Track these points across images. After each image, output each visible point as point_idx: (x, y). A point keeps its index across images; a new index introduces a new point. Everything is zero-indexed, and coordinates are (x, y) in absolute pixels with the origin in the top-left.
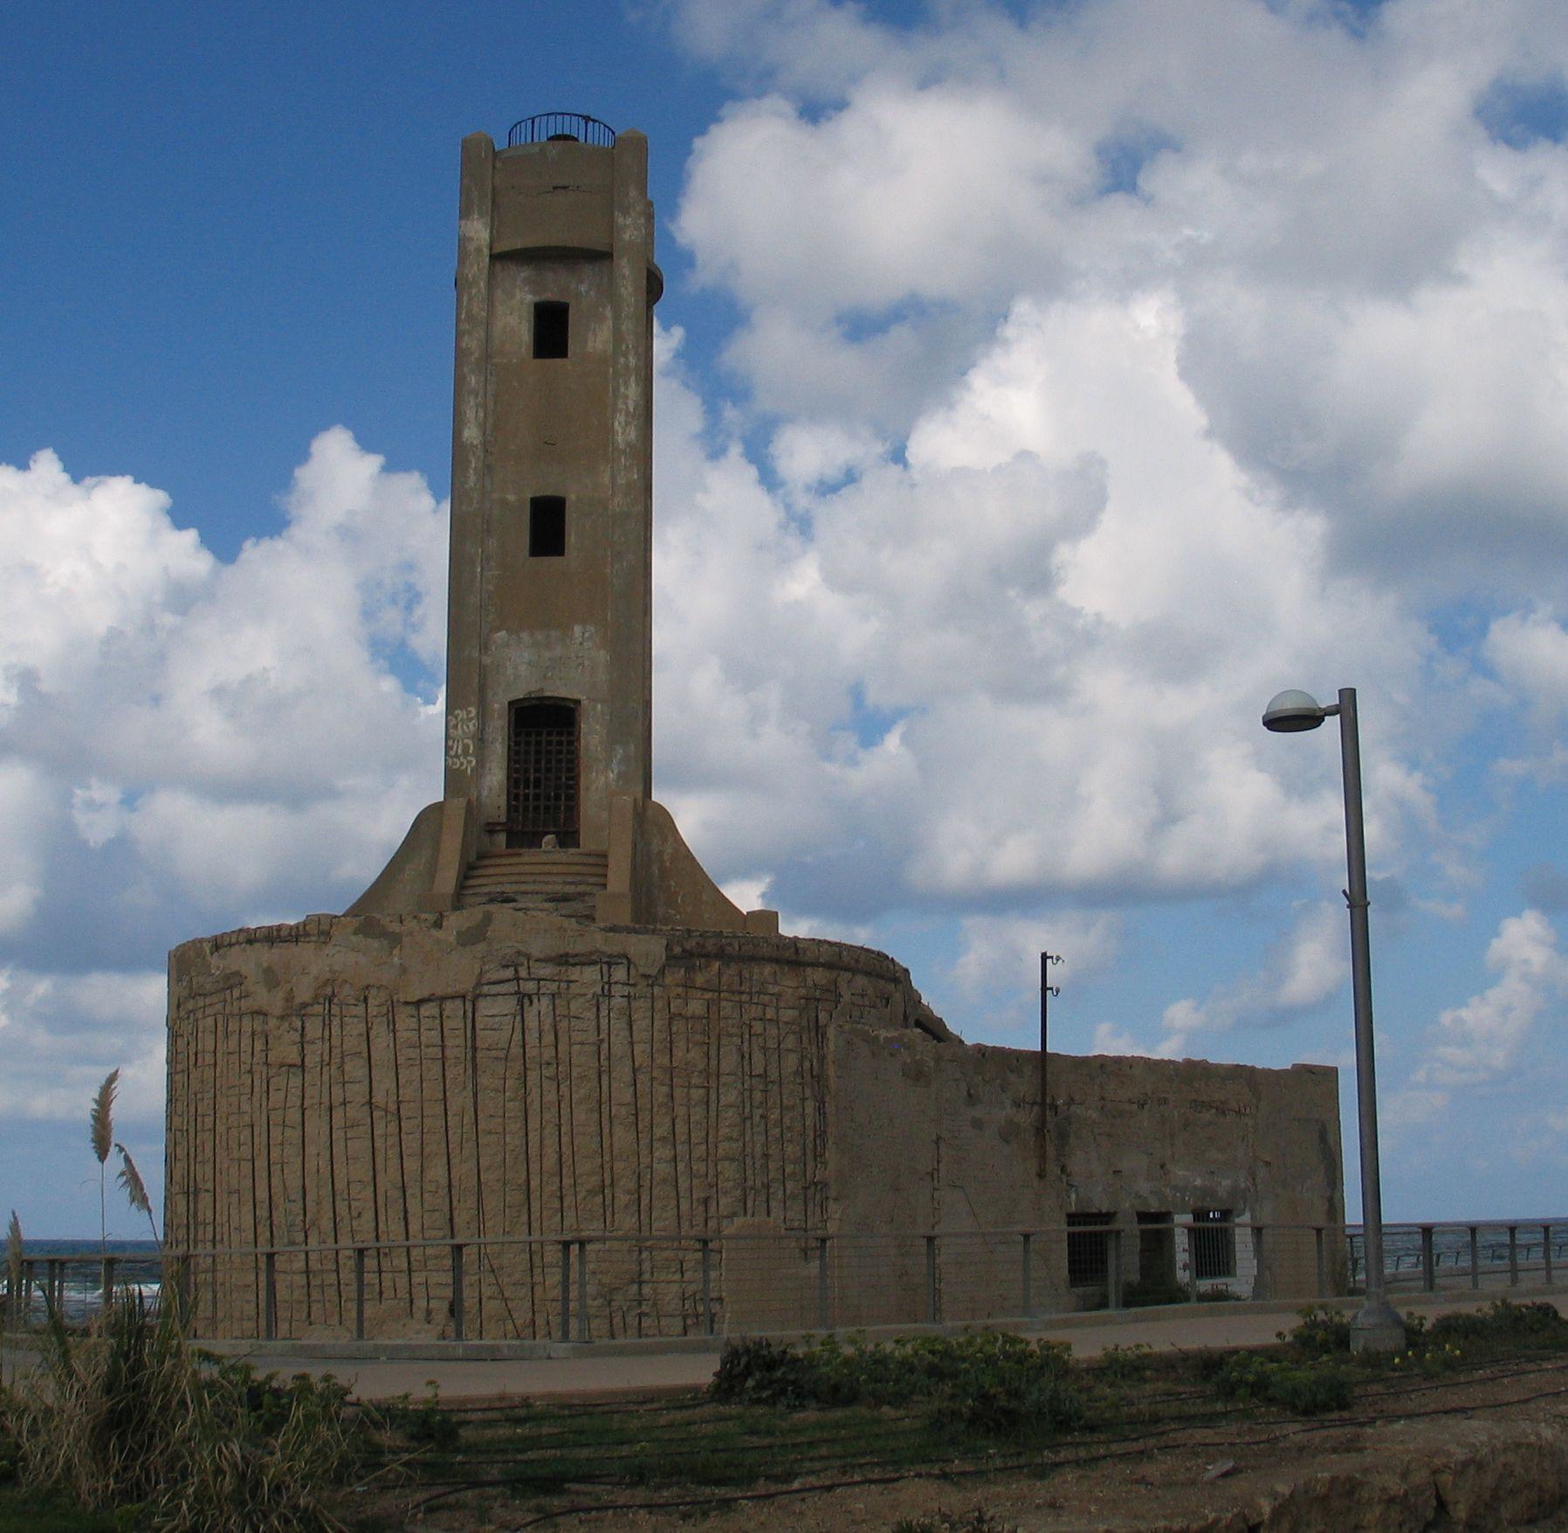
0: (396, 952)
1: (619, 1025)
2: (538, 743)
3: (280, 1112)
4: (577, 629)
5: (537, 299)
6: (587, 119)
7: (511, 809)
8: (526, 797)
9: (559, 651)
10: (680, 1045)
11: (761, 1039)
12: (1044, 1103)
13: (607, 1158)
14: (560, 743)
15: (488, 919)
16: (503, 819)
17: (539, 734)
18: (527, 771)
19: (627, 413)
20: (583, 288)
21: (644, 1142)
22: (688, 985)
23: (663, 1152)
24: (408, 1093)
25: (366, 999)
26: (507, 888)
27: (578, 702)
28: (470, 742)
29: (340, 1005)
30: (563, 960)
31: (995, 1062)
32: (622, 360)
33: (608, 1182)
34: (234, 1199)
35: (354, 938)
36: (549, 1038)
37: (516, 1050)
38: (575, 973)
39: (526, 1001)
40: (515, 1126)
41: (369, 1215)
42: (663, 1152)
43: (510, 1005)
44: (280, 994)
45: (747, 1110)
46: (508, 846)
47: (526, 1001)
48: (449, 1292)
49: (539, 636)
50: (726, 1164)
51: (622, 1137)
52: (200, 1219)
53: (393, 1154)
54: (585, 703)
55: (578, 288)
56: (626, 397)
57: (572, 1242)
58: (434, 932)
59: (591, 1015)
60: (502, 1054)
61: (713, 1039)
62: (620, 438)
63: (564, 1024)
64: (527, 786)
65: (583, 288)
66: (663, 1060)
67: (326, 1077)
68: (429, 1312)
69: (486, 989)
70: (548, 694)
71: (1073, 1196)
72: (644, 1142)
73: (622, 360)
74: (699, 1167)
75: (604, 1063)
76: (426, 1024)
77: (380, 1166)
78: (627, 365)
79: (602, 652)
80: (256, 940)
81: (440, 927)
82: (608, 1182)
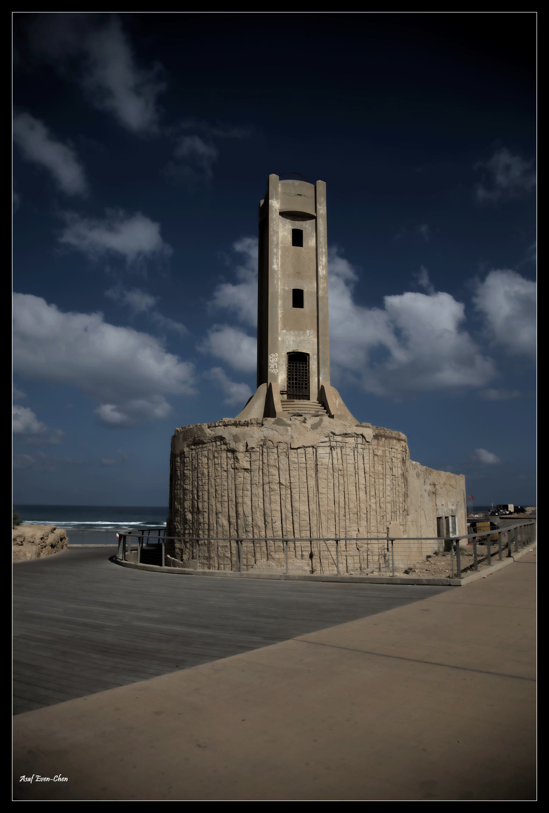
1: (360, 458)
2: (296, 366)
4: (308, 331)
5: (293, 228)
7: (288, 387)
8: (293, 383)
9: (302, 338)
10: (376, 464)
14: (303, 367)
16: (286, 390)
17: (296, 364)
18: (293, 375)
19: (323, 266)
20: (307, 226)
22: (378, 445)
26: (300, 412)
27: (308, 355)
29: (267, 448)
30: (346, 435)
36: (340, 461)
37: (330, 466)
38: (348, 440)
40: (331, 492)
42: (373, 500)
43: (328, 450)
49: (296, 333)
51: (362, 494)
54: (311, 355)
55: (306, 226)
58: (303, 424)
59: (352, 454)
60: (326, 467)
63: (344, 457)
64: (293, 380)
65: (307, 226)
66: (372, 469)
68: (302, 556)
70: (299, 351)
74: (382, 505)
75: (357, 470)
76: (300, 456)
78: (322, 252)
80: (228, 425)
81: (305, 422)
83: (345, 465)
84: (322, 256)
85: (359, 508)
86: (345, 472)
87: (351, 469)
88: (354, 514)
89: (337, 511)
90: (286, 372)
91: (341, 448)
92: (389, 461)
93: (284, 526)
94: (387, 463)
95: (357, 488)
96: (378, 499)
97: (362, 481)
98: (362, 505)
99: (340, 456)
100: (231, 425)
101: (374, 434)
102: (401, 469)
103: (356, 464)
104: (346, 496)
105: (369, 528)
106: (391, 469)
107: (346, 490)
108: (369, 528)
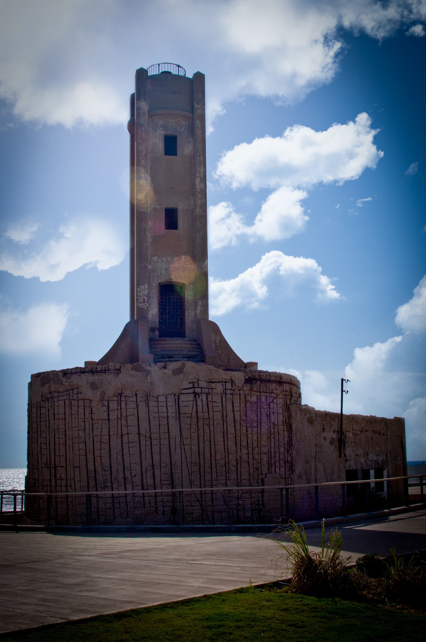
0: (148, 377)
2: (170, 299)
3: (99, 437)
5: (165, 133)
6: (179, 66)
8: (166, 318)
11: (272, 409)
12: (341, 432)
13: (226, 453)
15: (183, 366)
16: (158, 326)
18: (166, 309)
19: (201, 178)
21: (239, 447)
22: (251, 390)
23: (245, 451)
24: (155, 429)
25: (136, 395)
28: (146, 298)
31: (326, 416)
32: (198, 158)
33: (227, 462)
34: (77, 470)
35: (131, 372)
37: (194, 414)
39: (197, 396)
40: (195, 442)
41: (139, 476)
44: (99, 393)
45: (269, 436)
46: (159, 337)
47: (197, 396)
48: (171, 504)
50: (264, 455)
52: (58, 477)
53: (149, 453)
56: (200, 172)
57: (284, 488)
60: (190, 415)
61: (259, 409)
62: (198, 187)
63: (210, 404)
67: (119, 425)
69: (183, 391)
71: (347, 464)
72: (239, 447)
73: (198, 158)
74: (256, 456)
75: (225, 418)
77: (143, 456)
79: (192, 266)
82: (227, 462)
83: (211, 413)
84: (200, 167)
85: (227, 460)
86: (211, 421)
87: (218, 416)
88: (221, 466)
89: (202, 463)
90: (157, 306)
91: (207, 394)
92: (265, 407)
93: (145, 481)
94: (262, 410)
95: (226, 439)
96: (250, 449)
97: (231, 430)
98: (231, 457)
99: (205, 402)
100: (87, 372)
101: (247, 377)
102: (283, 416)
103: (225, 412)
104: (213, 447)
105: (239, 481)
106: (268, 416)
107: (212, 439)
108: (239, 481)
